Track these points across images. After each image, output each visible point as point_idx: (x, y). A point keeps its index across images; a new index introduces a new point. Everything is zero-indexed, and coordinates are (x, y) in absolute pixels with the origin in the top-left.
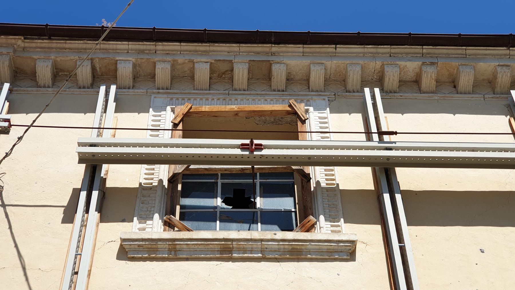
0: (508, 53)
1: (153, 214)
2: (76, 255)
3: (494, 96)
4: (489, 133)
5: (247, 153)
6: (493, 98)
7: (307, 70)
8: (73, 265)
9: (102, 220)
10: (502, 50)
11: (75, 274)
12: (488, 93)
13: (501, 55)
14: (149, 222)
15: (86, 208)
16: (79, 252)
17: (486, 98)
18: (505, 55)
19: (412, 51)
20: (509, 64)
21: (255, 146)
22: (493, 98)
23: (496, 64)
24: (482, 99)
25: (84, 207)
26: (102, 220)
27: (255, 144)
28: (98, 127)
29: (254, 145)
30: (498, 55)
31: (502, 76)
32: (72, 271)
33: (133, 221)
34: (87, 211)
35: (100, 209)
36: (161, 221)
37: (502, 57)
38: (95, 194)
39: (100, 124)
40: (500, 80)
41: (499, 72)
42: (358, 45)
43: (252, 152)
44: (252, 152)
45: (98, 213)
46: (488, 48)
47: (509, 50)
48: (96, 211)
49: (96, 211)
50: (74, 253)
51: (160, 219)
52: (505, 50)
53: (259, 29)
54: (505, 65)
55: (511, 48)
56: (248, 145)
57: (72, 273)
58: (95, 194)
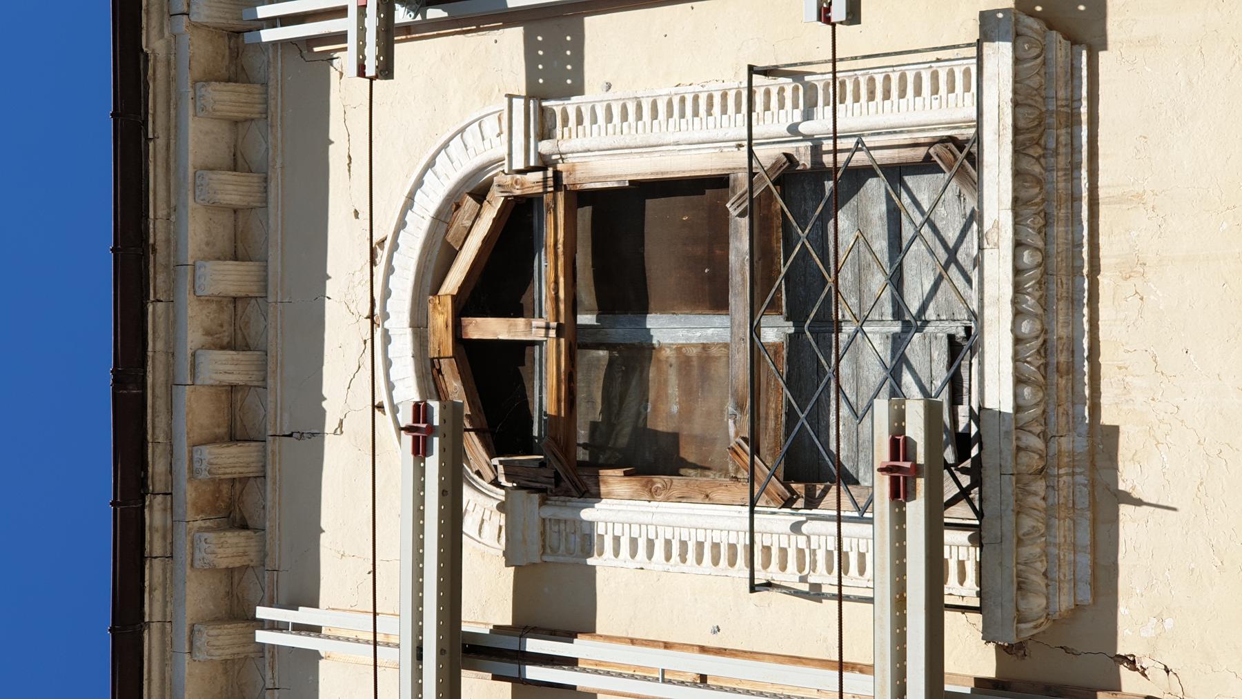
0: (159, 624)
1: (582, 521)
2: (664, 681)
3: (269, 666)
4: (373, 149)
5: (436, 440)
6: (273, 668)
7: (219, 426)
8: (687, 688)
9: (588, 629)
10: (152, 642)
11: (706, 682)
12: (259, 670)
13: (163, 642)
14: (600, 529)
15: (565, 665)
16: (657, 676)
17: (274, 683)
18: (163, 632)
19: (161, 193)
20: (187, 630)
21: (419, 423)
22: (273, 668)
23: (187, 662)
24: (277, 695)
25: (564, 669)
26: (588, 629)
27: (414, 422)
28: (377, 640)
29: (416, 425)
30: (163, 652)
31: (218, 648)
32: (700, 687)
33: (594, 567)
34: (571, 663)
35: (568, 636)
36: (596, 505)
37: (170, 640)
38: (534, 645)
39: (367, 642)
40: (227, 651)
41: (209, 658)
42: (145, 372)
43: (431, 430)
44: (431, 430)
45: (576, 637)
46: (145, 676)
47: (151, 624)
48: (572, 642)
49: (572, 642)
50: (660, 685)
51: (593, 507)
52: (152, 634)
53: (109, 369)
54: (190, 638)
55: (147, 619)
56: (416, 440)
57: (703, 688)
58: (534, 645)
